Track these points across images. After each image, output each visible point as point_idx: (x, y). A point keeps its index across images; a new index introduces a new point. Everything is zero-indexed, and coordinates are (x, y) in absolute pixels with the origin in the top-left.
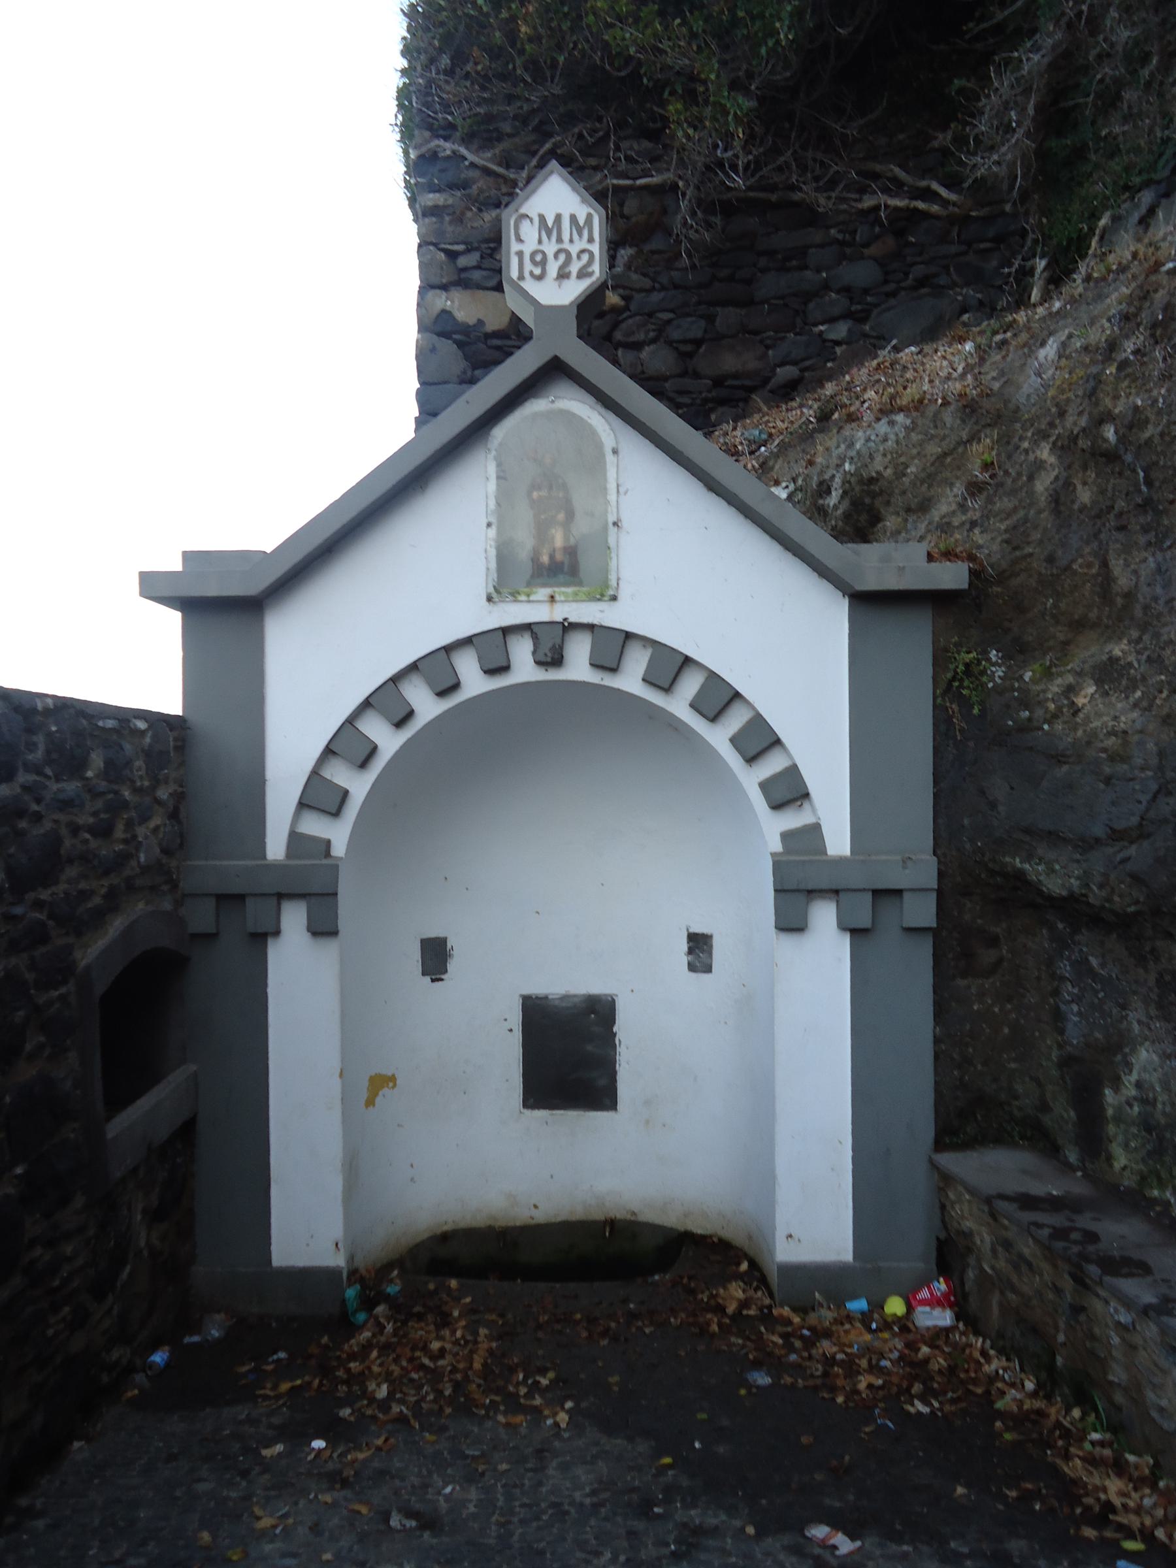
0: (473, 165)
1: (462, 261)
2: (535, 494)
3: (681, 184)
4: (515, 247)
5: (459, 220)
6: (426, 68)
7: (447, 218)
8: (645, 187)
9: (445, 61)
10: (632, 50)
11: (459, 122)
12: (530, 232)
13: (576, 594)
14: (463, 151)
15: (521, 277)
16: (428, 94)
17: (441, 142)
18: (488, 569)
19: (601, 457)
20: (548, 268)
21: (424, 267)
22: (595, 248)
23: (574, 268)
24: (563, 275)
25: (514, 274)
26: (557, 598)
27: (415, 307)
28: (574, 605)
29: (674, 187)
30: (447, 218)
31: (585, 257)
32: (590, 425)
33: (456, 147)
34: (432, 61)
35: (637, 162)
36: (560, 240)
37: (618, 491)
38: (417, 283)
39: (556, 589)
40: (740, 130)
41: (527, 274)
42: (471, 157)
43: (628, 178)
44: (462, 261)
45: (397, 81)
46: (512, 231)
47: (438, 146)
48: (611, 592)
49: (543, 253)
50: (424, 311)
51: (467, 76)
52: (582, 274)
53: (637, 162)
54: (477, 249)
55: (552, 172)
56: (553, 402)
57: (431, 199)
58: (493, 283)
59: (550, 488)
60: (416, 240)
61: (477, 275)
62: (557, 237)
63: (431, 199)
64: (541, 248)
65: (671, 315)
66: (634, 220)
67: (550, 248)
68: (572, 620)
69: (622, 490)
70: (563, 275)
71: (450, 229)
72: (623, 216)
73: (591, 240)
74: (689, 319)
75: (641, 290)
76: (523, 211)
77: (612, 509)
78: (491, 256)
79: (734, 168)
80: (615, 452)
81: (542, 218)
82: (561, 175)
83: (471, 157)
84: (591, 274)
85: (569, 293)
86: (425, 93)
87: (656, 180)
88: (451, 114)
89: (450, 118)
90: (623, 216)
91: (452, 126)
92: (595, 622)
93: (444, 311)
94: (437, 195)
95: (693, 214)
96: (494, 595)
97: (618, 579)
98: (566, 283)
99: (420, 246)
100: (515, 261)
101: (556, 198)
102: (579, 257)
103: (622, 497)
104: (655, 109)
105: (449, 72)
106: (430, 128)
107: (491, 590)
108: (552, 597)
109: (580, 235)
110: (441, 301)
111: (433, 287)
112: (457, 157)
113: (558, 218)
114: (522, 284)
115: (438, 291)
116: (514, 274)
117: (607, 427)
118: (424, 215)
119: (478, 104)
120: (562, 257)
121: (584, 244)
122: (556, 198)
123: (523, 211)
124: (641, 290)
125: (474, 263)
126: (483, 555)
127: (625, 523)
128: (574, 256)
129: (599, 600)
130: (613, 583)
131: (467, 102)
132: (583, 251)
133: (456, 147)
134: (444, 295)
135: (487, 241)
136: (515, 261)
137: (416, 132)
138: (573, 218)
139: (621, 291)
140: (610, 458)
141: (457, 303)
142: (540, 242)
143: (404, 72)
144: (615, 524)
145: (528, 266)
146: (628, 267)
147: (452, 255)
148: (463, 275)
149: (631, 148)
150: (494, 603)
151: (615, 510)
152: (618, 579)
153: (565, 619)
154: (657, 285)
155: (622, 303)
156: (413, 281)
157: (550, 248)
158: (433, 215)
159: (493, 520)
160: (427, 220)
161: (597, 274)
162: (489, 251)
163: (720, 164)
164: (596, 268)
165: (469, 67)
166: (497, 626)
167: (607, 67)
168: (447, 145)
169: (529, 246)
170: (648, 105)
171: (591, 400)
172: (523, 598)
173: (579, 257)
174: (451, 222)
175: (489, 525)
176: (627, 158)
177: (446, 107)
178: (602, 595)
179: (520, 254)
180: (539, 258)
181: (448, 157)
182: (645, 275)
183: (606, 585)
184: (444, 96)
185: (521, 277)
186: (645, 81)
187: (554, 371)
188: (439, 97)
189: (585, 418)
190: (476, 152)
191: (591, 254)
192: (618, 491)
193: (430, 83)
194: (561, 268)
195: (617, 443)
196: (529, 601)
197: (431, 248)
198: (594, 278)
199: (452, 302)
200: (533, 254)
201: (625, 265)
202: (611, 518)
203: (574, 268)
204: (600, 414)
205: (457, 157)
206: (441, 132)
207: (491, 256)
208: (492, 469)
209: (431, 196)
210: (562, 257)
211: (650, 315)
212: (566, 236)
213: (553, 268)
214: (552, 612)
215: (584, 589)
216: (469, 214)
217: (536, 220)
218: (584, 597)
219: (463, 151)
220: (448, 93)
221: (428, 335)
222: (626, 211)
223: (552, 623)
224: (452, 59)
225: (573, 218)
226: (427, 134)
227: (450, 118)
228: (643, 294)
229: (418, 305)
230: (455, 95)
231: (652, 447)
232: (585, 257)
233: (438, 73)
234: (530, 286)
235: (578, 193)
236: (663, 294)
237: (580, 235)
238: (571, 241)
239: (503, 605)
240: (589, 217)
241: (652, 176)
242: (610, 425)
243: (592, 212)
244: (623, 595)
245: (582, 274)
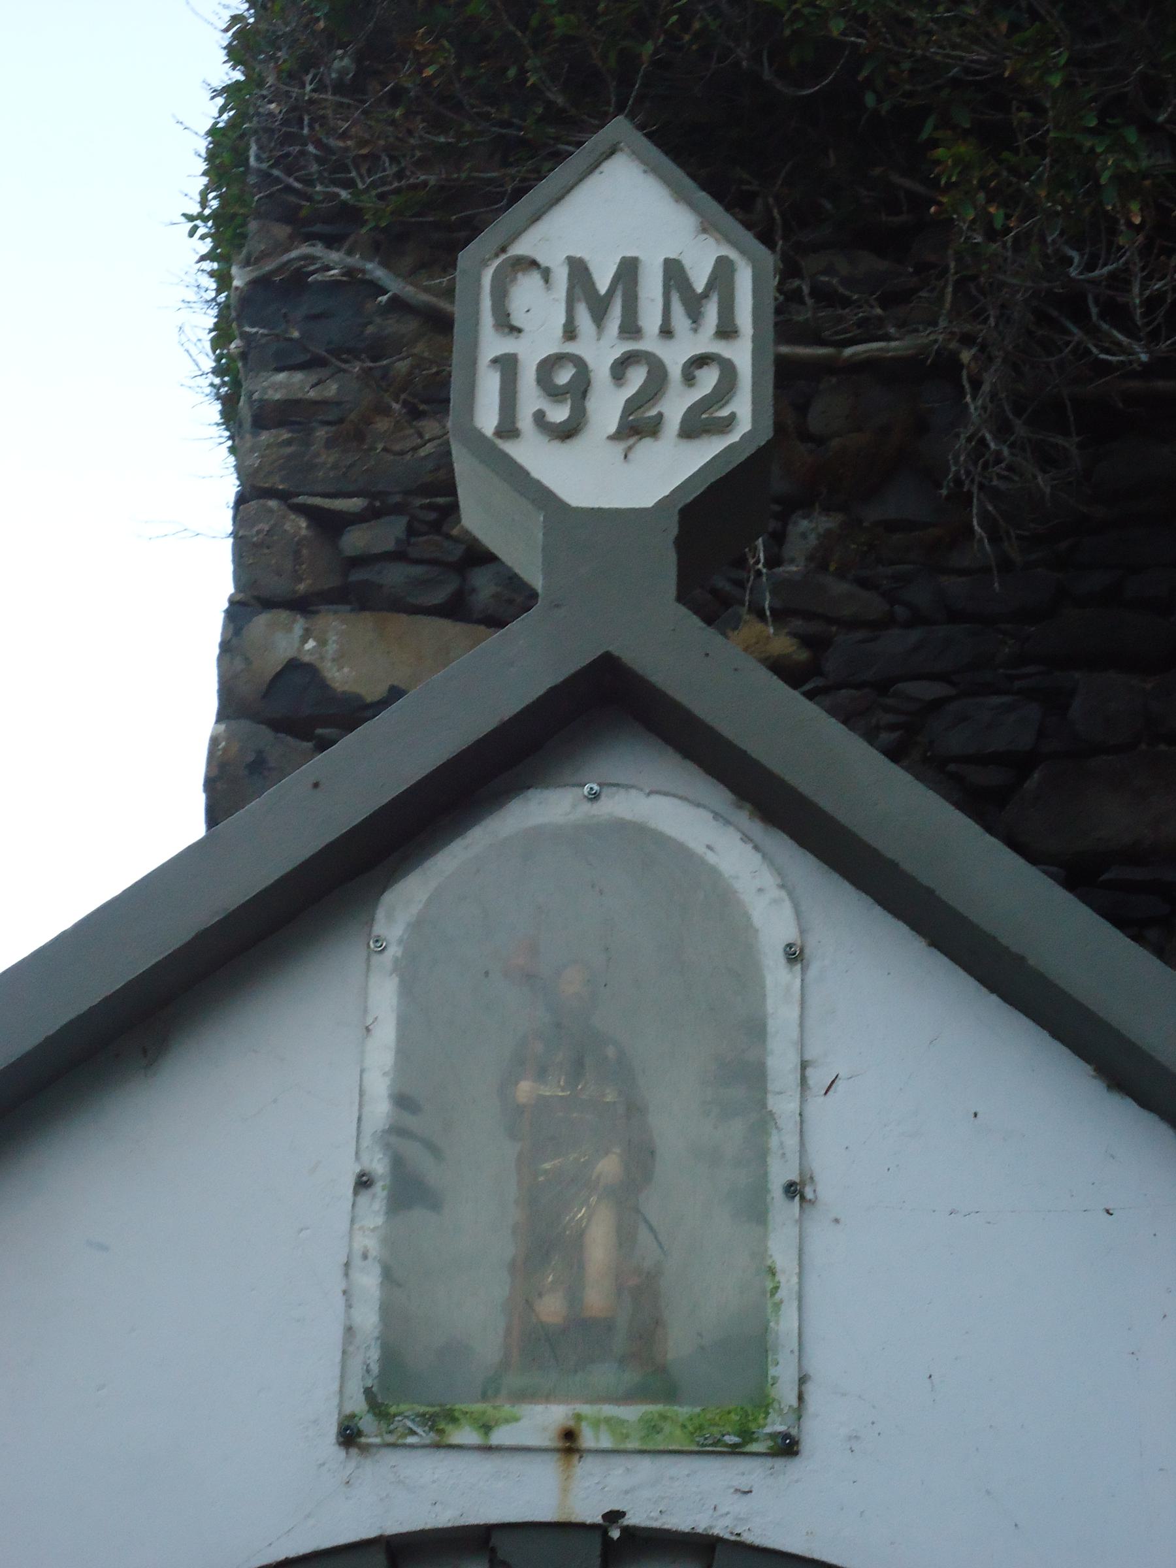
0: (398, 305)
1: (356, 540)
2: (525, 1089)
3: (966, 356)
4: (492, 345)
5: (352, 434)
6: (293, 77)
7: (321, 433)
8: (869, 365)
9: (341, 63)
10: (837, 27)
11: (368, 202)
12: (540, 311)
13: (652, 1427)
14: (376, 271)
15: (508, 430)
16: (289, 138)
17: (318, 250)
18: (349, 1330)
19: (744, 973)
20: (592, 404)
21: (247, 550)
22: (741, 354)
23: (675, 406)
24: (637, 427)
25: (487, 419)
26: (588, 1439)
27: (216, 651)
28: (646, 1467)
29: (945, 368)
30: (321, 433)
31: (709, 379)
32: (714, 871)
33: (355, 261)
34: (308, 62)
35: (846, 302)
36: (631, 329)
37: (803, 1080)
38: (227, 588)
39: (586, 1409)
40: (1135, 207)
41: (525, 422)
42: (395, 285)
43: (823, 343)
44: (356, 540)
45: (207, 112)
46: (486, 304)
47: (312, 259)
48: (776, 1425)
49: (580, 364)
50: (239, 664)
51: (396, 97)
52: (696, 426)
53: (846, 302)
54: (398, 509)
55: (612, 152)
56: (595, 797)
57: (280, 384)
58: (439, 596)
59: (577, 1069)
60: (230, 486)
61: (395, 576)
62: (620, 326)
63: (280, 384)
64: (571, 348)
65: (937, 690)
66: (835, 443)
67: (600, 350)
68: (634, 1518)
69: (818, 1078)
70: (637, 427)
71: (329, 458)
72: (805, 436)
73: (727, 331)
74: (996, 700)
75: (852, 624)
76: (521, 248)
77: (784, 1139)
78: (435, 527)
79: (1117, 314)
80: (794, 956)
81: (579, 270)
82: (637, 155)
83: (395, 285)
84: (729, 423)
85: (665, 471)
86: (283, 137)
87: (896, 346)
88: (349, 184)
89: (344, 194)
90: (805, 436)
91: (350, 215)
92: (720, 1529)
93: (294, 666)
94: (298, 376)
95: (1003, 429)
96: (367, 1423)
97: (803, 1380)
98: (646, 448)
99: (241, 500)
100: (489, 385)
101: (623, 213)
102: (689, 379)
103: (817, 1103)
104: (896, 179)
105: (351, 88)
106: (289, 216)
107: (357, 1404)
108: (569, 1435)
109: (695, 316)
110: (285, 640)
111: (268, 604)
112: (354, 282)
113: (629, 270)
114: (511, 448)
115: (283, 615)
116: (487, 419)
117: (768, 879)
118: (260, 423)
119: (422, 164)
120: (637, 377)
121: (705, 342)
122: (623, 213)
123: (521, 248)
124: (852, 624)
125: (390, 546)
126: (340, 1285)
127: (826, 1189)
128: (675, 371)
129: (735, 1451)
130: (786, 1393)
131: (393, 159)
132: (701, 361)
133: (355, 261)
134: (300, 625)
135: (427, 490)
136: (489, 385)
137: (253, 226)
138: (674, 272)
139: (798, 624)
140: (778, 977)
141: (332, 648)
142: (570, 333)
143: (231, 92)
144: (793, 1190)
145: (530, 399)
146: (819, 561)
147: (329, 525)
148: (356, 576)
149: (829, 270)
150: (365, 1449)
151: (792, 1141)
152: (803, 1380)
153: (613, 1516)
154: (900, 611)
155: (803, 655)
156: (214, 580)
157: (600, 350)
158: (281, 424)
159: (379, 1165)
160: (265, 436)
161: (745, 424)
162: (432, 516)
163: (1074, 304)
164: (742, 408)
165: (405, 77)
166: (368, 1532)
167: (767, 75)
168: (334, 256)
169: (533, 350)
170: (877, 171)
171: (720, 796)
172: (466, 1435)
173: (689, 379)
174: (330, 443)
175: (363, 1182)
176: (816, 292)
177: (337, 168)
178: (747, 1436)
179: (508, 365)
180: (564, 376)
181: (334, 284)
182: (863, 583)
183: (763, 1403)
184: (334, 143)
185: (508, 430)
186: (870, 99)
187: (602, 706)
188: (318, 144)
189: (700, 849)
190: (410, 275)
191: (728, 370)
192: (803, 1080)
193: (295, 114)
194: (633, 406)
195: (802, 932)
196: (488, 1449)
197: (273, 503)
198: (734, 437)
199: (322, 642)
200: (548, 366)
201: (810, 558)
202: (780, 1173)
203: (675, 406)
204: (746, 838)
205: (354, 282)
206: (318, 228)
207: (435, 527)
208: (385, 997)
209: (281, 377)
210: (637, 377)
211: (883, 686)
212: (650, 317)
213: (607, 407)
214: (565, 1491)
215: (683, 1411)
216: (382, 425)
217: (561, 276)
218: (679, 1440)
219: (376, 271)
220: (344, 136)
221: (245, 725)
222: (815, 422)
223: (564, 1529)
224: (359, 59)
225: (674, 272)
226: (281, 231)
227: (344, 194)
228: (860, 635)
229: (226, 648)
230: (362, 143)
231: (918, 945)
232: (709, 379)
233: (320, 88)
234: (534, 455)
235: (692, 205)
236: (915, 635)
237: (695, 316)
238: (666, 332)
239: (392, 1458)
240: (723, 273)
241: (887, 338)
242: (779, 872)
243: (733, 255)
244: (817, 1434)
245: (696, 426)
